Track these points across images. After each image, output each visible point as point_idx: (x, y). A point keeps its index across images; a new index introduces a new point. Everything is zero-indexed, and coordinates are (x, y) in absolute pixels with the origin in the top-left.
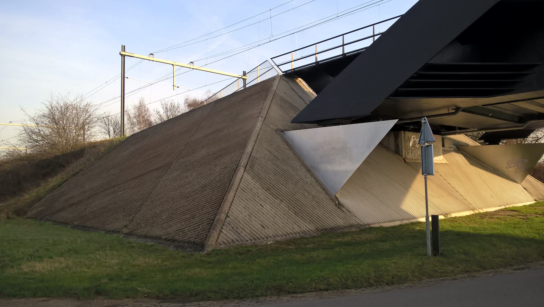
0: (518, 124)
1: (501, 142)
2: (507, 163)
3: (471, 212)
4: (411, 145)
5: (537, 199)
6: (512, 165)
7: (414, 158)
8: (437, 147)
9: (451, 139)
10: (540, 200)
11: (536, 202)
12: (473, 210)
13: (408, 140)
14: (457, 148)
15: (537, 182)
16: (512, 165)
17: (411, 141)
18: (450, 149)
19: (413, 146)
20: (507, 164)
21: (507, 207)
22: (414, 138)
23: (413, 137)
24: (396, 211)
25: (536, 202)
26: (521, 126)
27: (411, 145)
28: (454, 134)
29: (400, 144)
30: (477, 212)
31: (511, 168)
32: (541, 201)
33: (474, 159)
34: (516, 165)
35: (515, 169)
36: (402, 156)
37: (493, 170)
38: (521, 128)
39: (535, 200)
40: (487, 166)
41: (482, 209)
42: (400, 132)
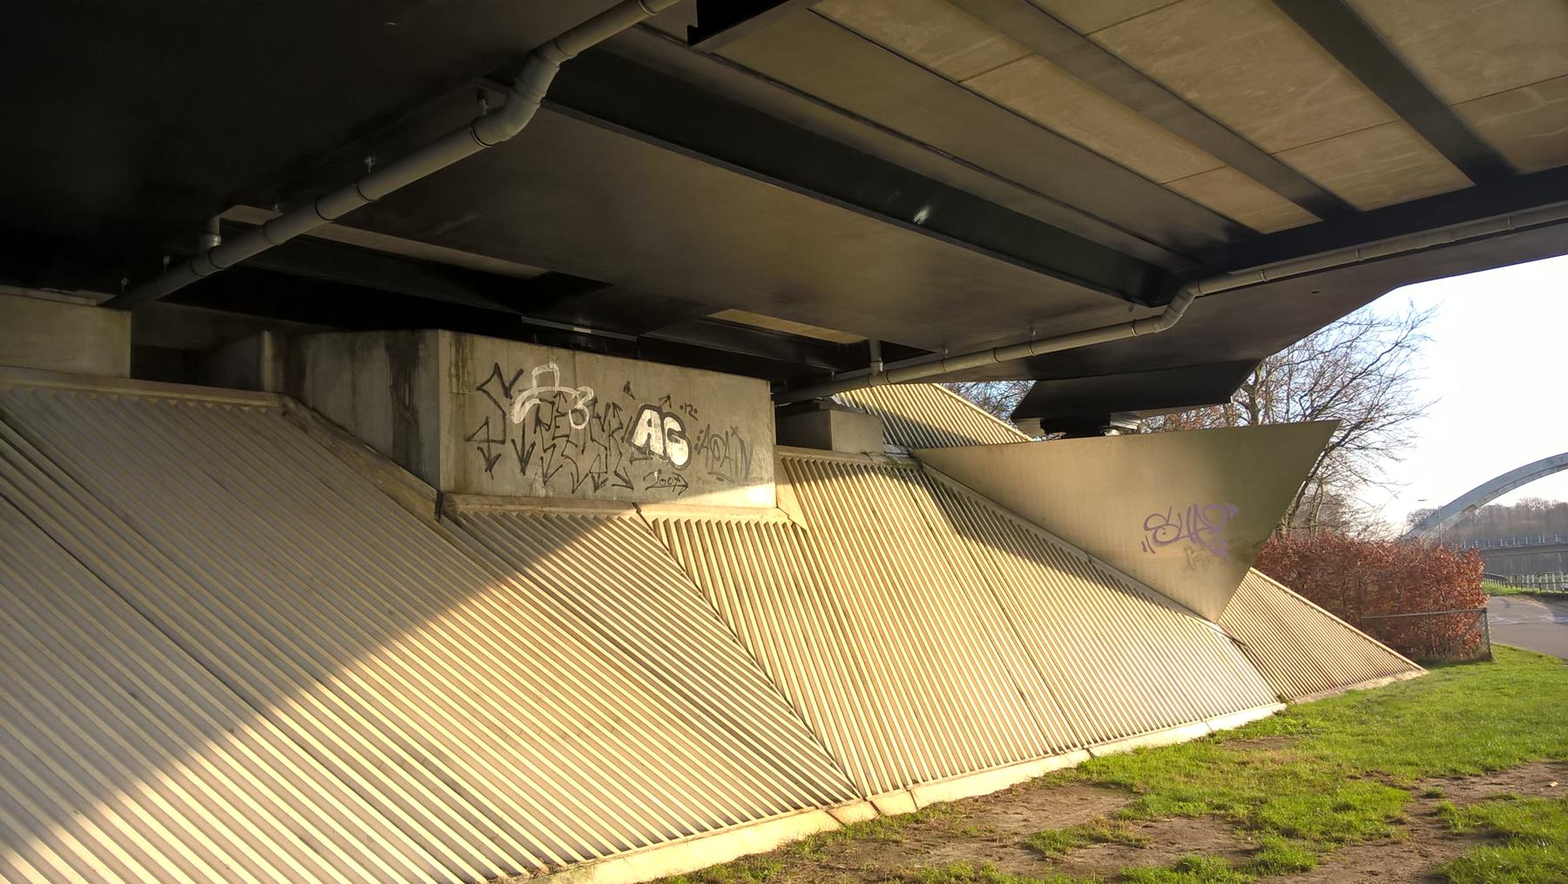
0: (1141, 311)
1: (1116, 428)
2: (1146, 524)
3: (813, 822)
4: (520, 412)
5: (1288, 689)
6: (1171, 533)
7: (542, 492)
8: (734, 442)
9: (863, 412)
10: (1305, 693)
11: (1282, 707)
12: (828, 803)
13: (494, 388)
14: (911, 456)
15: (1305, 609)
16: (1171, 533)
17: (526, 394)
18: (863, 461)
19: (538, 422)
20: (1147, 529)
21: (1099, 751)
22: (546, 379)
23: (536, 372)
24: (1155, 670)
25: (1282, 707)
26: (1157, 318)
27: (520, 412)
28: (866, 381)
29: (423, 406)
30: (856, 812)
31: (1168, 548)
32: (1310, 699)
33: (991, 507)
34: (1185, 532)
35: (1185, 549)
36: (432, 481)
37: (1084, 558)
38: (1158, 328)
39: (1281, 699)
40: (1051, 539)
41: (908, 785)
42: (429, 334)
